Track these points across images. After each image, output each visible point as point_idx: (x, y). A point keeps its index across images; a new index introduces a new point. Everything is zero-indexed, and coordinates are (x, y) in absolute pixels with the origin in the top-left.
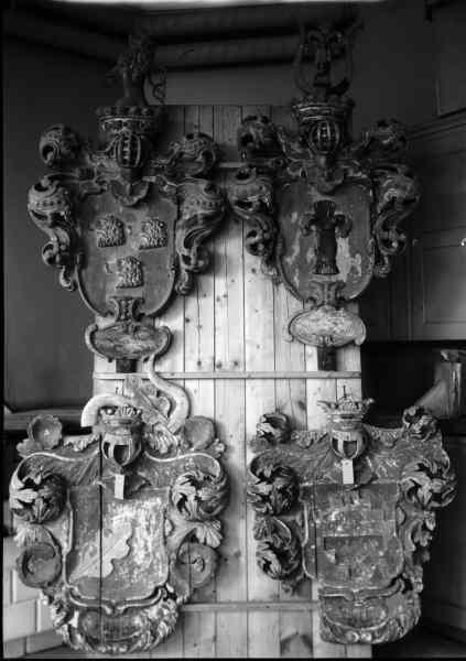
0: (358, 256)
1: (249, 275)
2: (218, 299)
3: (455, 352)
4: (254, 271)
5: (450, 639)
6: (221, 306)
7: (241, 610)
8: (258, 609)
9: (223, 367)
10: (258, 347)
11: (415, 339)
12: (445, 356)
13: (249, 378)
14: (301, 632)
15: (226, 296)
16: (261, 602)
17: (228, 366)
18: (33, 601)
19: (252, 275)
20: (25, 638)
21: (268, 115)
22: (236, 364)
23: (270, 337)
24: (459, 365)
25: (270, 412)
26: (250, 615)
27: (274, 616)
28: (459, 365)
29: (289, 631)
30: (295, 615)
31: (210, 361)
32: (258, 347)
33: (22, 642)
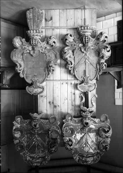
0: (65, 52)
1: (59, 105)
2: (67, 99)
3: (4, 86)
4: (58, 106)
5: (13, 22)
6: (66, 97)
7: (61, 27)
8: (58, 27)
9: (65, 83)
10: (57, 88)
11: (18, 90)
12: (7, 86)
13: (59, 80)
14: (47, 22)
15: (65, 100)
16: (57, 29)
17: (65, 83)
18: (103, 28)
19: (59, 105)
20: (105, 20)
21: (17, 42)
22: (62, 84)
23: (90, 65)
24: (4, 83)
25: (58, 67)
26: (59, 26)
27: (54, 25)
28: (4, 83)
29: (50, 22)
30: (49, 26)
31: (69, 84)
32: (57, 88)
33: (106, 19)
